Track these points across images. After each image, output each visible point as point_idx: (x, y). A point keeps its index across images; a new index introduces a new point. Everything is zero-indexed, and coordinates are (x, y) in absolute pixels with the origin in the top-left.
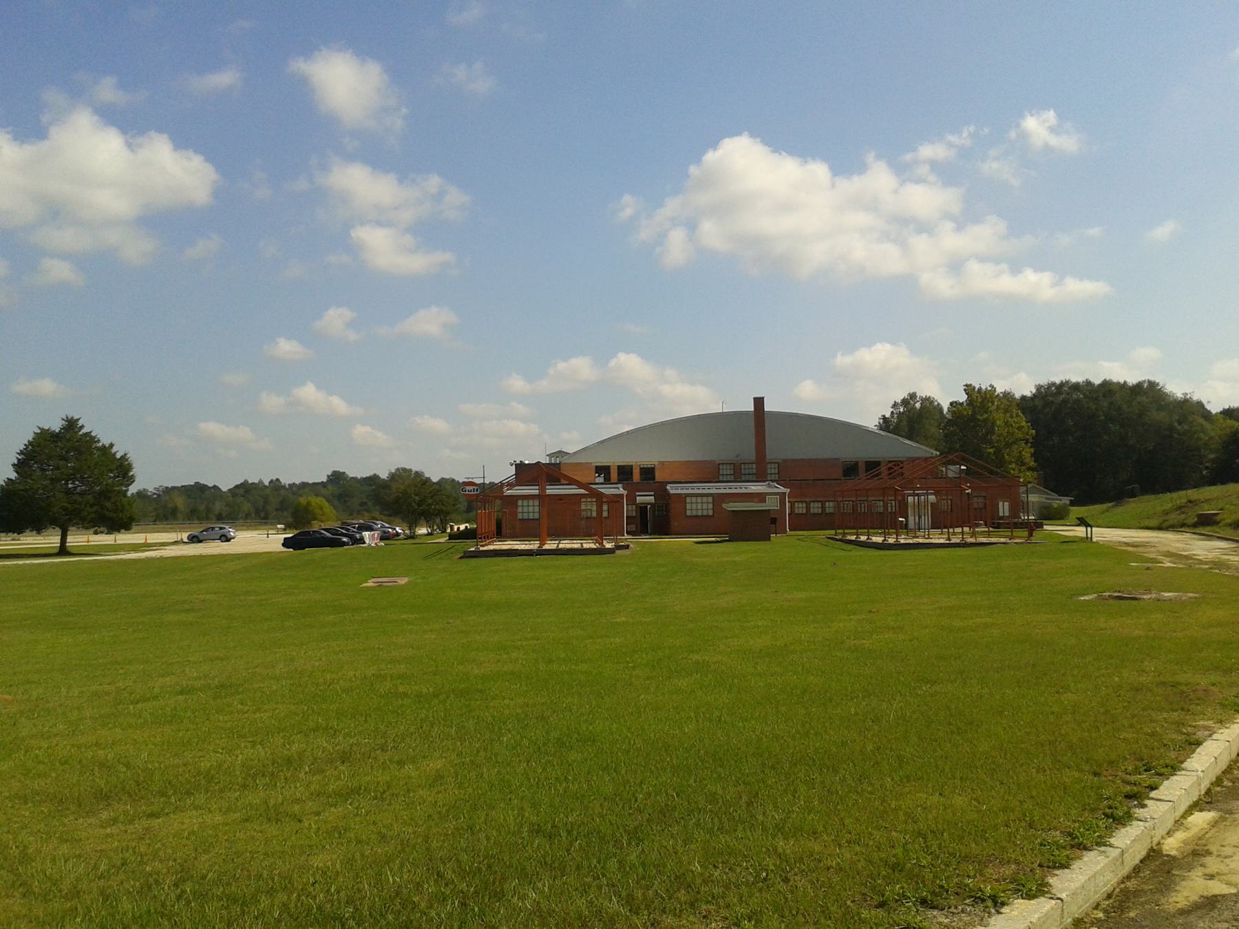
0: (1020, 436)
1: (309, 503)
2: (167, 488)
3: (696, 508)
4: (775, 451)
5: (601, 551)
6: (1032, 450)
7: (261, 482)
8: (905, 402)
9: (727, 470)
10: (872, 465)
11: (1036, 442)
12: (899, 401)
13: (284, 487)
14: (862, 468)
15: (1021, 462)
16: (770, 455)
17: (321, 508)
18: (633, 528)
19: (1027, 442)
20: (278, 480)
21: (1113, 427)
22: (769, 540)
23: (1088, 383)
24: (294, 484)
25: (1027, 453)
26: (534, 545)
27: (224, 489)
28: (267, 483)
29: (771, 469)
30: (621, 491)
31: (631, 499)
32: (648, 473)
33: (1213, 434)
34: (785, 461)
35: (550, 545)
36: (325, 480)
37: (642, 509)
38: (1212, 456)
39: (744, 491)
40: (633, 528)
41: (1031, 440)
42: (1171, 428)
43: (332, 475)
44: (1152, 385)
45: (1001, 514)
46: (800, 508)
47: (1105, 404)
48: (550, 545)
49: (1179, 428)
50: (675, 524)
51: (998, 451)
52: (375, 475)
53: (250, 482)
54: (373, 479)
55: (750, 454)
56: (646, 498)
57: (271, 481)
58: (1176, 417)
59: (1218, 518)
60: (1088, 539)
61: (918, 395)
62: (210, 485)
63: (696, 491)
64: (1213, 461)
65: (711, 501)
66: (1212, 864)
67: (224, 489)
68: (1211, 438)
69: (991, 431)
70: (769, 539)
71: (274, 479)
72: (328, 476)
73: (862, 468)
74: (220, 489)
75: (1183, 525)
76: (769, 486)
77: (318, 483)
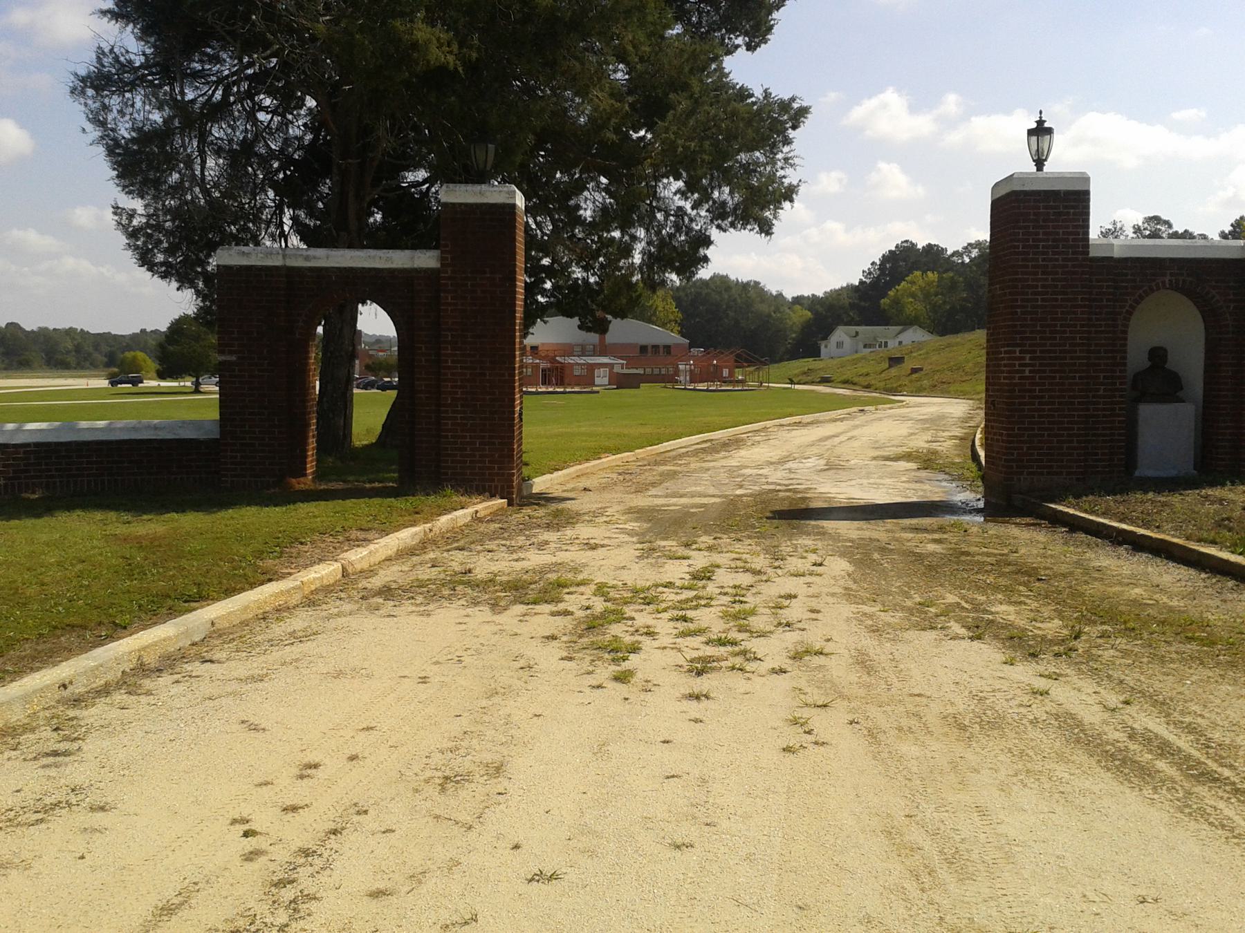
1: (135, 358)
9: (578, 349)
10: (656, 347)
17: (145, 361)
19: (676, 321)
21: (731, 314)
26: (562, 390)
33: (795, 320)
38: (794, 335)
39: (600, 362)
41: (679, 321)
42: (769, 316)
44: (757, 283)
45: (724, 375)
47: (726, 297)
49: (774, 315)
58: (773, 308)
59: (832, 379)
60: (791, 388)
64: (794, 339)
65: (655, 373)
66: (675, 632)
68: (794, 323)
70: (639, 387)
73: (650, 349)
75: (813, 382)
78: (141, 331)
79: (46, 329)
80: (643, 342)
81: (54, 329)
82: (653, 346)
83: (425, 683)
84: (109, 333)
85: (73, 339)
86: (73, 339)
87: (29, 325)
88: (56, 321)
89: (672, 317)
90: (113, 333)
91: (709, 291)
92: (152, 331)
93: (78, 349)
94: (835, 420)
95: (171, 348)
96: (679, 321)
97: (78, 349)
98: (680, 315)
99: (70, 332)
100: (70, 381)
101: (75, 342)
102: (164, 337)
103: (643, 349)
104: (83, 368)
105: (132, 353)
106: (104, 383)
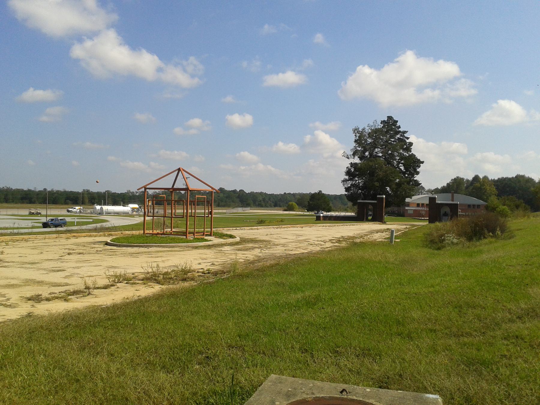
1: (292, 204)
10: (474, 206)
44: (458, 177)
78: (284, 193)
79: (253, 192)
80: (469, 203)
81: (256, 192)
82: (473, 205)
83: (2, 254)
84: (273, 194)
85: (262, 196)
86: (262, 196)
87: (247, 191)
88: (257, 190)
89: (493, 193)
90: (275, 194)
91: (511, 182)
92: (288, 193)
93: (264, 200)
94: (391, 224)
95: (311, 202)
96: (497, 195)
97: (264, 200)
98: (497, 192)
99: (261, 193)
100: (273, 211)
101: (263, 197)
102: (519, 209)
103: (469, 206)
104: (267, 207)
105: (291, 203)
106: (426, 223)
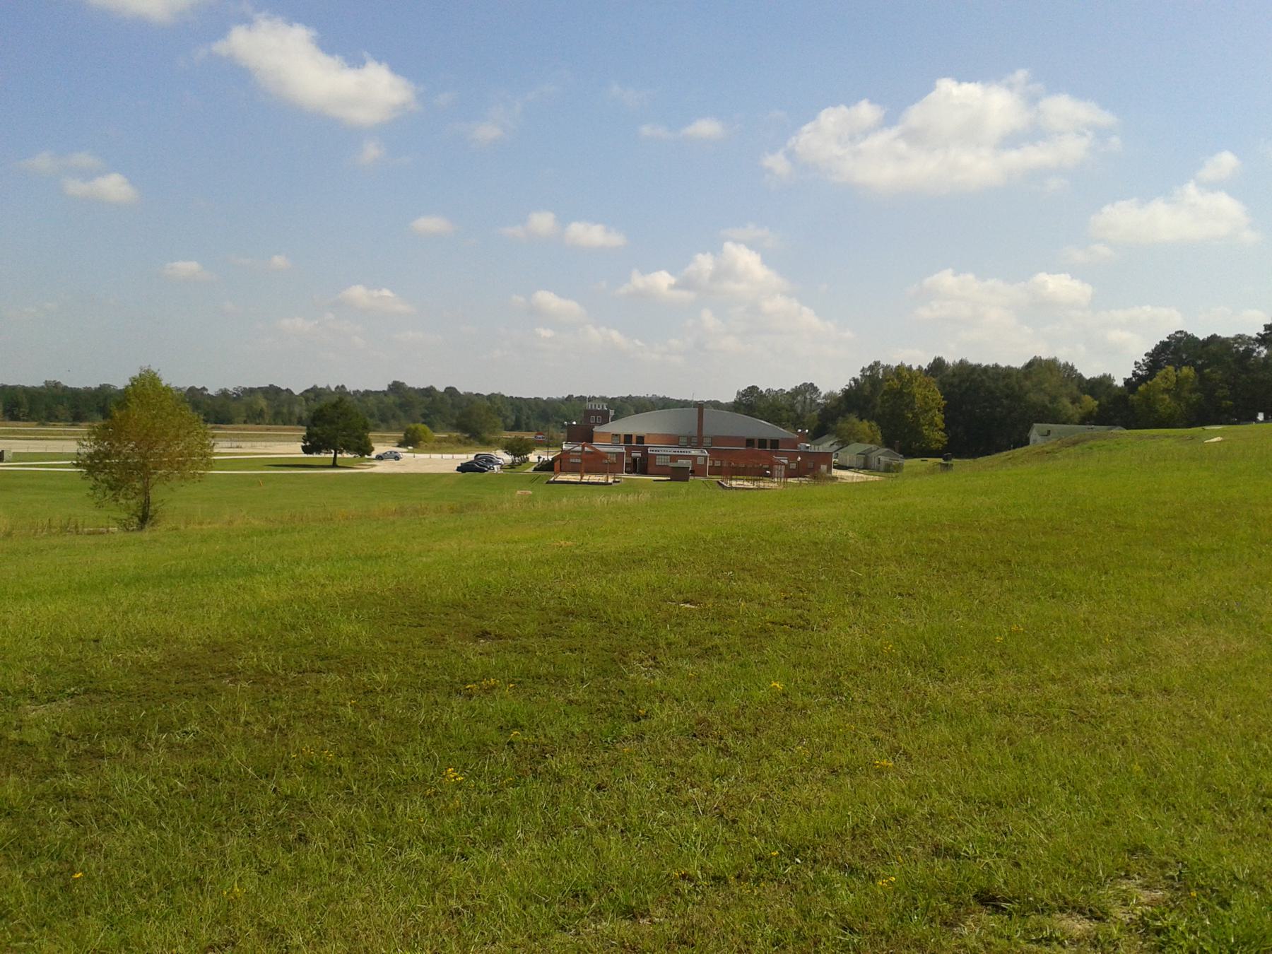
0: (934, 405)
1: (417, 429)
2: (245, 388)
3: (659, 461)
4: (708, 430)
5: (606, 484)
6: (943, 416)
7: (328, 387)
8: (871, 368)
9: (683, 440)
11: (946, 410)
12: (867, 366)
13: (349, 393)
14: (756, 443)
15: (932, 424)
16: (704, 433)
17: (425, 433)
18: (629, 469)
20: (343, 386)
22: (687, 481)
23: (997, 366)
24: (358, 391)
25: (939, 418)
27: (297, 392)
28: (333, 389)
29: (707, 441)
30: (624, 451)
31: (629, 454)
32: (641, 439)
34: (716, 436)
35: (586, 478)
36: (386, 388)
37: (635, 460)
40: (629, 469)
43: (393, 385)
46: (718, 464)
48: (586, 478)
50: (650, 469)
51: (916, 416)
52: (432, 387)
53: (319, 387)
54: (429, 391)
55: (695, 433)
56: (637, 454)
57: (337, 387)
61: (882, 363)
62: (284, 388)
63: (660, 453)
67: (297, 392)
69: (913, 402)
71: (340, 385)
72: (389, 386)
74: (292, 393)
76: (702, 451)
77: (380, 392)
